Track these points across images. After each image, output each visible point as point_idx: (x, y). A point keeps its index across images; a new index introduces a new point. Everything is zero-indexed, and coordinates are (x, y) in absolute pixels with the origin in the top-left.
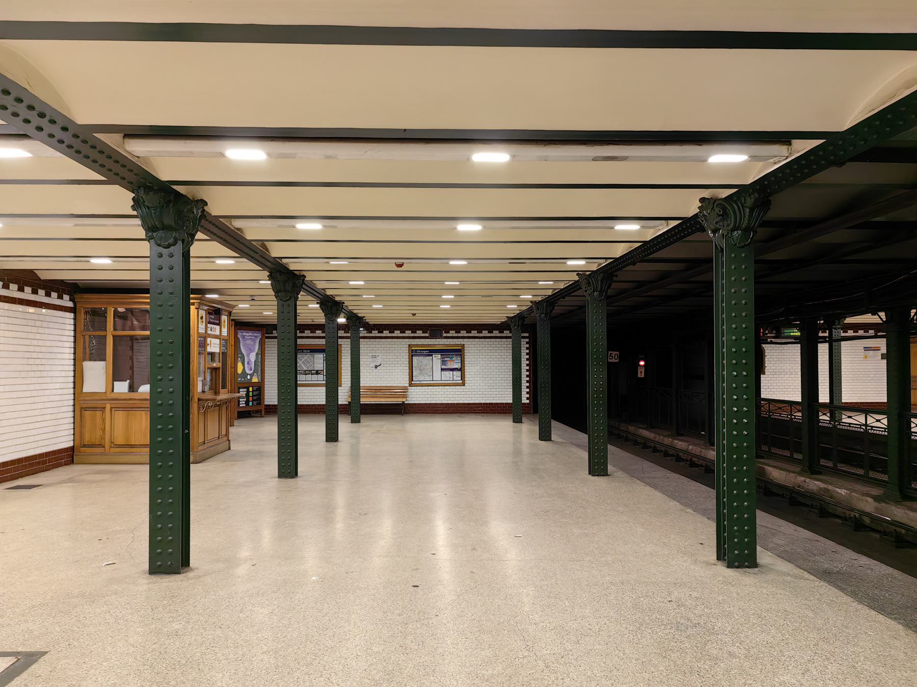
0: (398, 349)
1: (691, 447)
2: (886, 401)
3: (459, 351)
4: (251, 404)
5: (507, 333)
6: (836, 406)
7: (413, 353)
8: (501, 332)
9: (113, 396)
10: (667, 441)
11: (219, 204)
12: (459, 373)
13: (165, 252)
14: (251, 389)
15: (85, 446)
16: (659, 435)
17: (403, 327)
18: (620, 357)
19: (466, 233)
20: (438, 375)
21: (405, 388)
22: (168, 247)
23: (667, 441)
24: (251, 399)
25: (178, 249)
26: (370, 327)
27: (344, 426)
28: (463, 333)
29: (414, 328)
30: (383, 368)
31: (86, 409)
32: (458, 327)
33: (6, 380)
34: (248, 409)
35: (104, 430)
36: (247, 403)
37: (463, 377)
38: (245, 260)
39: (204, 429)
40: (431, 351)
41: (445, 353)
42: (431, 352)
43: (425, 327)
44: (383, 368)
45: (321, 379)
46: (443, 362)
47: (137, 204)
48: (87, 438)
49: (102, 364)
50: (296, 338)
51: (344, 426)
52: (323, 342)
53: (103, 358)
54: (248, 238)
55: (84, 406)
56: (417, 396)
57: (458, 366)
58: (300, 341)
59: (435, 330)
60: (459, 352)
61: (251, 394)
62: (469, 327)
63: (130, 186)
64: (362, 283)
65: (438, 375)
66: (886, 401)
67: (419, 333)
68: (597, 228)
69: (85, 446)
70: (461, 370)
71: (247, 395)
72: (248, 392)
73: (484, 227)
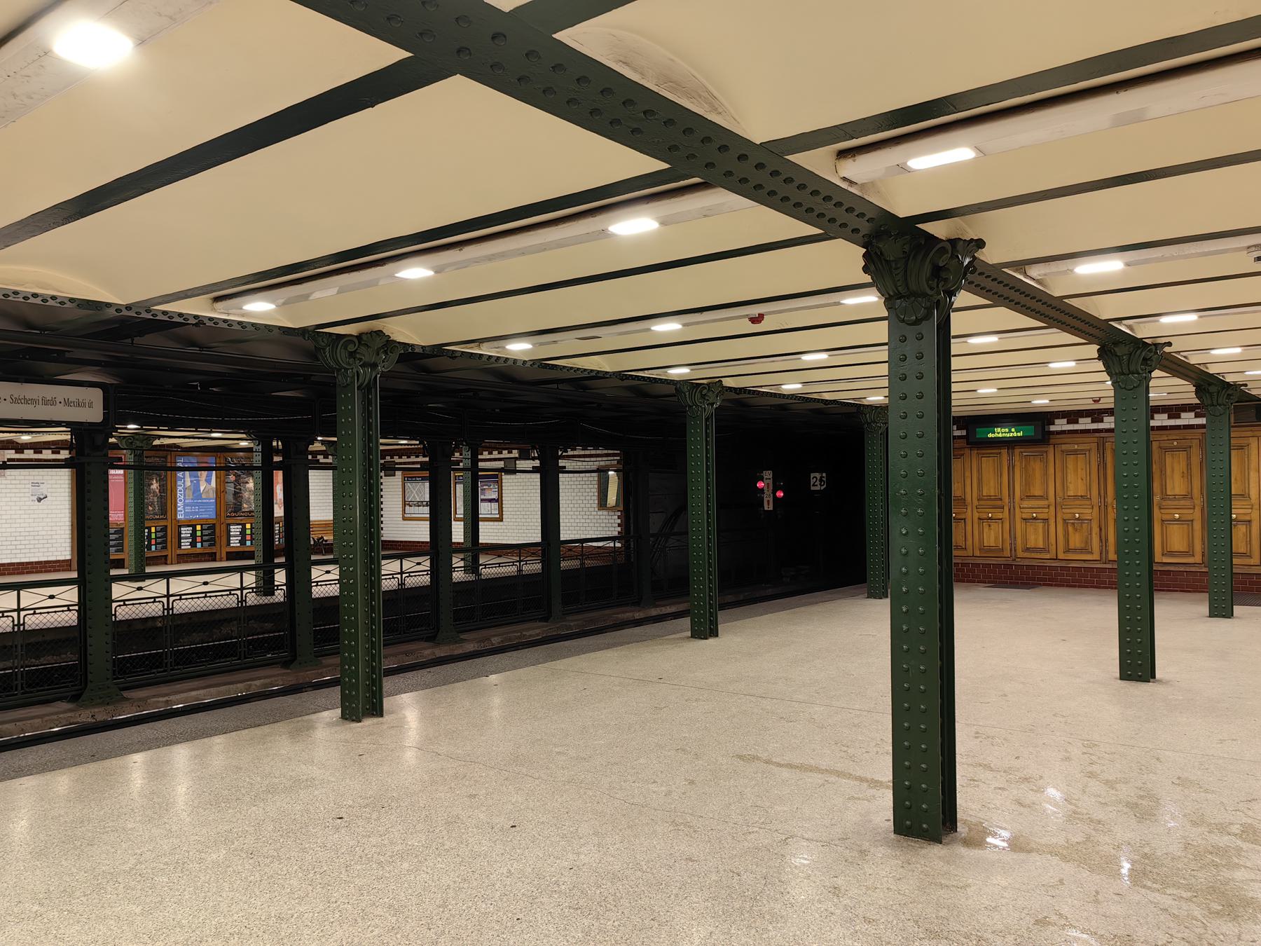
2: (538, 539)
4: (199, 545)
6: (474, 548)
11: (1004, 242)
12: (495, 505)
13: (910, 332)
14: (199, 528)
19: (639, 242)
22: (917, 322)
24: (199, 539)
25: (930, 329)
27: (1179, 625)
34: (194, 551)
36: (193, 544)
38: (1055, 330)
47: (873, 263)
51: (1179, 625)
54: (1057, 293)
57: (495, 496)
58: (481, 465)
61: (199, 533)
63: (852, 235)
64: (1239, 350)
66: (538, 539)
68: (503, 255)
70: (499, 500)
71: (243, 533)
72: (194, 531)
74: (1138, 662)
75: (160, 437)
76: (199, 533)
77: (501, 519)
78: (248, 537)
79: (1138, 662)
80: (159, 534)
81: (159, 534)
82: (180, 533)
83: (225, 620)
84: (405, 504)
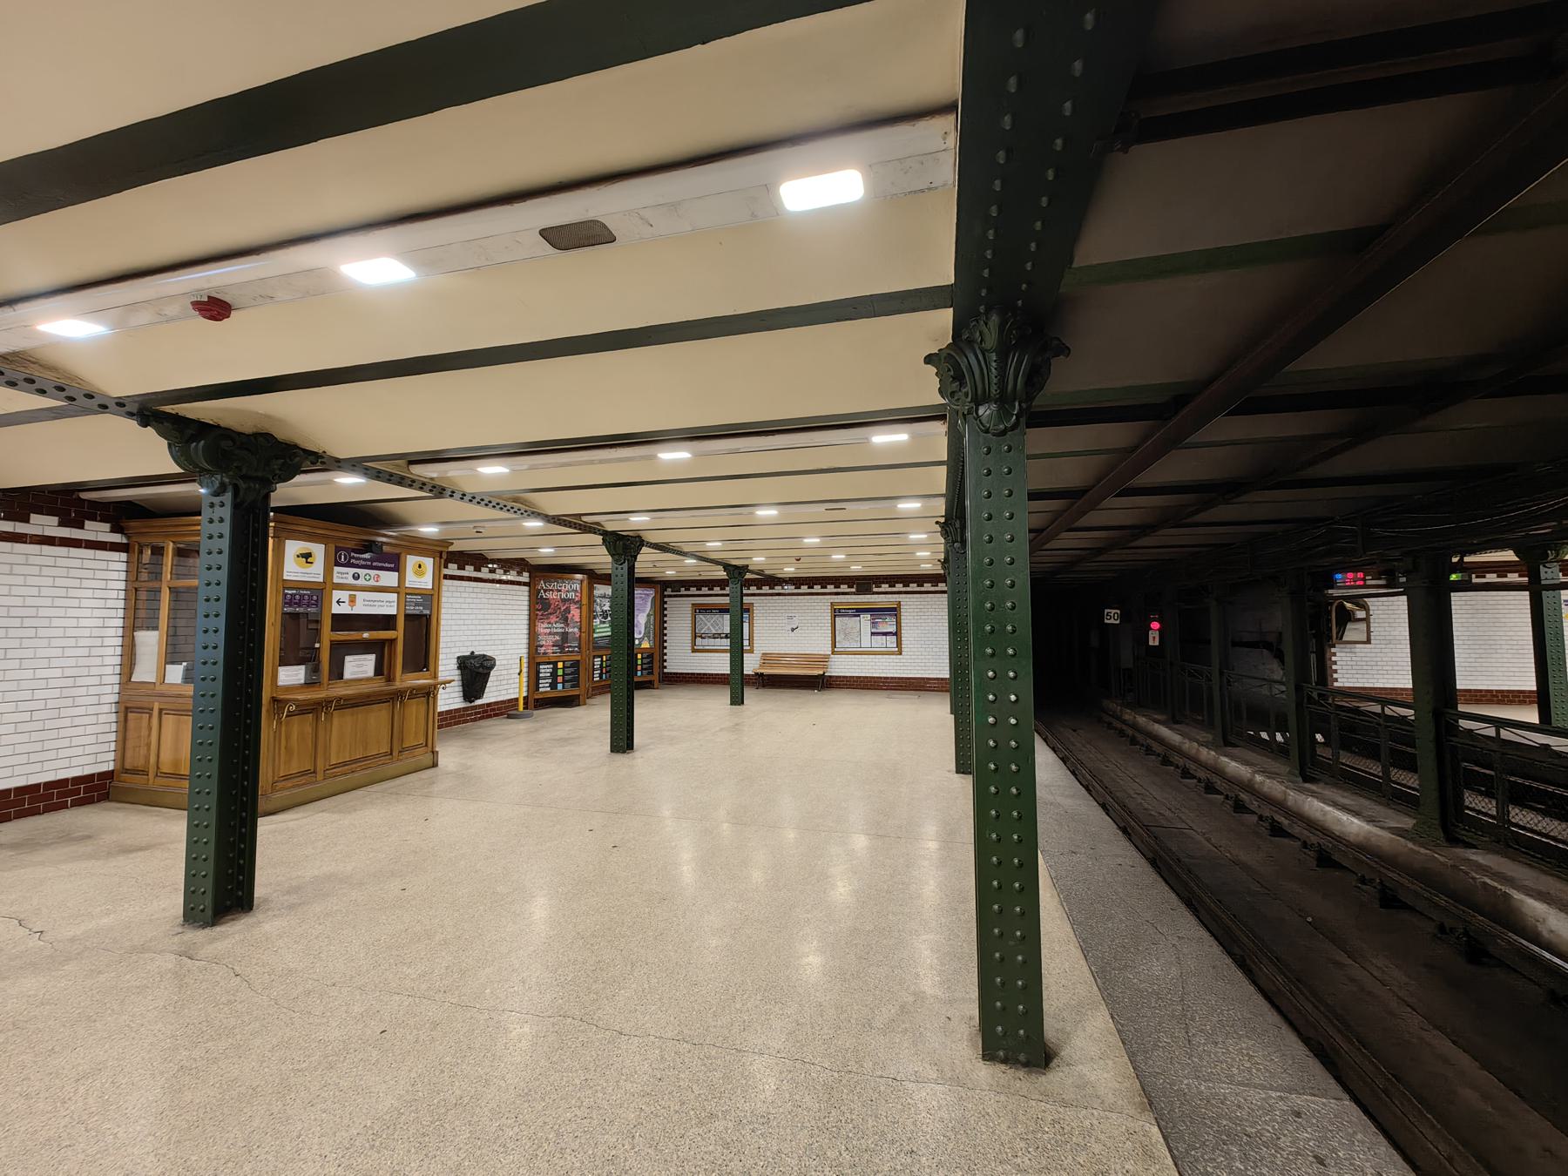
0: (818, 608)
1: (1258, 778)
3: (894, 609)
4: (560, 686)
5: (942, 586)
7: (837, 612)
8: (478, 569)
9: (163, 687)
10: (1207, 754)
14: (560, 665)
15: (127, 771)
16: (1192, 739)
17: (824, 581)
18: (1122, 617)
19: (675, 464)
20: (867, 641)
21: (827, 657)
23: (1207, 754)
24: (560, 679)
26: (771, 581)
28: (899, 587)
29: (837, 581)
30: (786, 632)
31: (1235, 644)
32: (892, 580)
33: (31, 656)
35: (149, 745)
36: (553, 686)
37: (899, 644)
39: (280, 750)
40: (859, 610)
41: (876, 612)
42: (859, 612)
43: (850, 580)
44: (786, 632)
45: (725, 643)
46: (874, 624)
48: (128, 766)
49: (156, 633)
50: (742, 595)
52: (726, 600)
53: (156, 628)
55: (133, 706)
56: (841, 667)
57: (893, 629)
59: (864, 584)
60: (894, 611)
61: (560, 672)
62: (906, 579)
65: (867, 641)
67: (844, 588)
69: (127, 771)
70: (897, 634)
71: (554, 675)
72: (555, 669)
73: (695, 455)
74: (623, 740)
75: (1020, 363)
76: (560, 672)
77: (1368, 641)
78: (560, 679)
79: (623, 740)
80: (568, 671)
81: (568, 671)
82: (538, 672)
83: (1509, 966)
84: (695, 636)
